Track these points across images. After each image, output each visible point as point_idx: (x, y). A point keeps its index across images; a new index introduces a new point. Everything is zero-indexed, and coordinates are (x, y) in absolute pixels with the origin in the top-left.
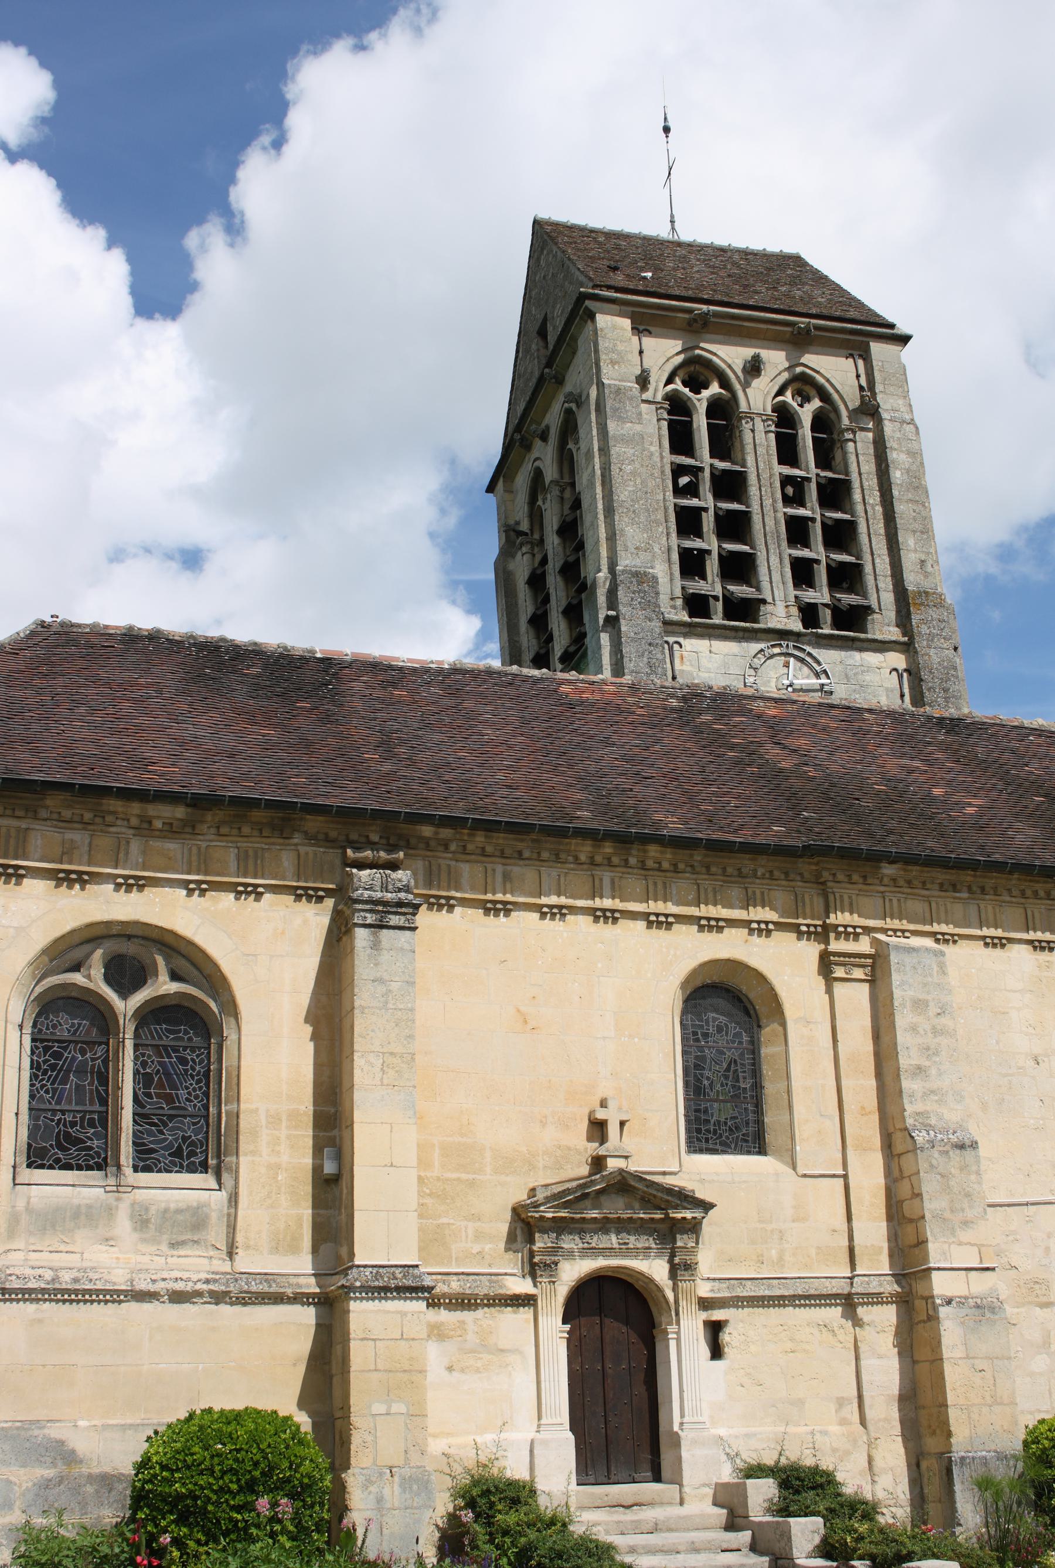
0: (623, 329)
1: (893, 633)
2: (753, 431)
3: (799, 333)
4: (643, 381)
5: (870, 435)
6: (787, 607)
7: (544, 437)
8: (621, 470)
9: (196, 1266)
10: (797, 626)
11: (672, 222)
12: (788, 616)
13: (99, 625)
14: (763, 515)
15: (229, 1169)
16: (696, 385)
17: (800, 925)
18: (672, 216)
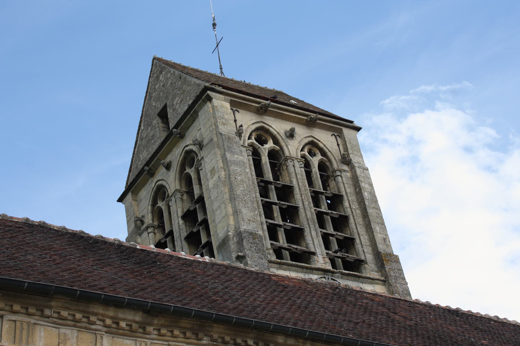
0: (226, 107)
1: (375, 275)
2: (294, 166)
3: (311, 120)
4: (239, 133)
5: (349, 174)
6: (323, 258)
7: (168, 167)
8: (236, 178)
10: (329, 267)
11: (221, 68)
12: (325, 263)
13: (7, 216)
14: (305, 209)
16: (262, 141)
18: (221, 66)
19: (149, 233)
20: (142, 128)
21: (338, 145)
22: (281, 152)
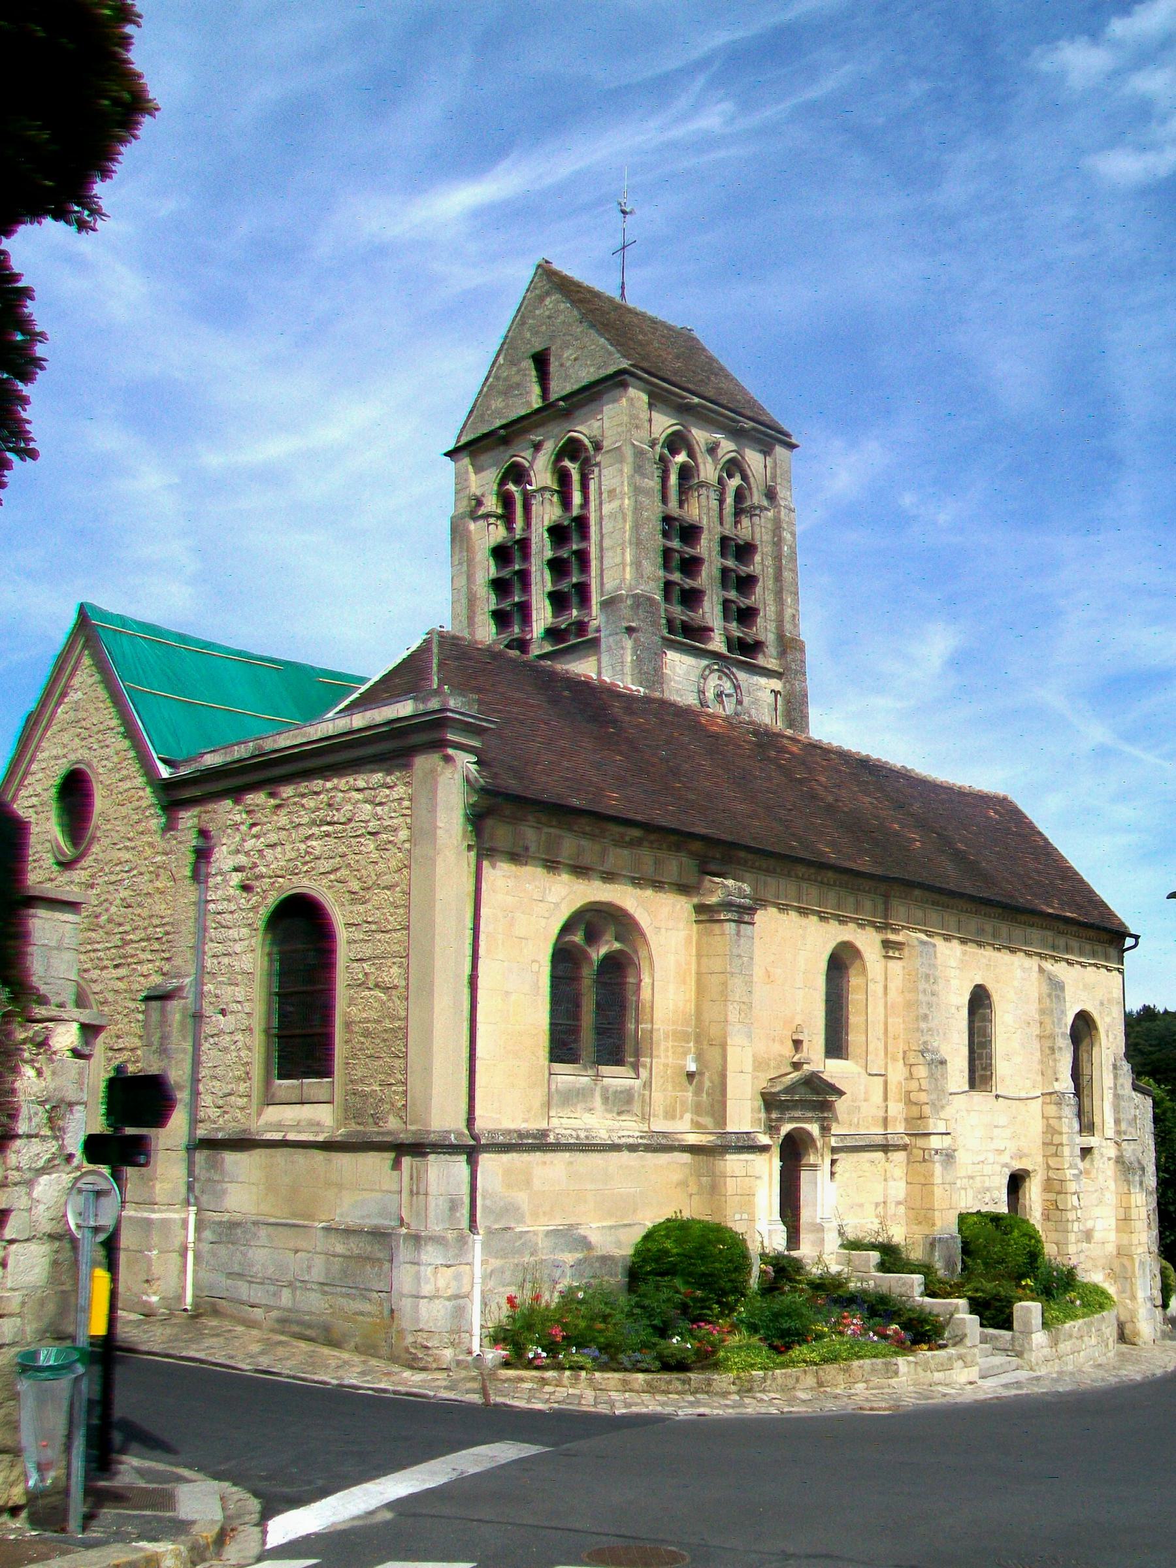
9: (629, 1128)
11: (623, 288)
15: (644, 1066)
16: (674, 452)
20: (501, 360)
22: (694, 470)
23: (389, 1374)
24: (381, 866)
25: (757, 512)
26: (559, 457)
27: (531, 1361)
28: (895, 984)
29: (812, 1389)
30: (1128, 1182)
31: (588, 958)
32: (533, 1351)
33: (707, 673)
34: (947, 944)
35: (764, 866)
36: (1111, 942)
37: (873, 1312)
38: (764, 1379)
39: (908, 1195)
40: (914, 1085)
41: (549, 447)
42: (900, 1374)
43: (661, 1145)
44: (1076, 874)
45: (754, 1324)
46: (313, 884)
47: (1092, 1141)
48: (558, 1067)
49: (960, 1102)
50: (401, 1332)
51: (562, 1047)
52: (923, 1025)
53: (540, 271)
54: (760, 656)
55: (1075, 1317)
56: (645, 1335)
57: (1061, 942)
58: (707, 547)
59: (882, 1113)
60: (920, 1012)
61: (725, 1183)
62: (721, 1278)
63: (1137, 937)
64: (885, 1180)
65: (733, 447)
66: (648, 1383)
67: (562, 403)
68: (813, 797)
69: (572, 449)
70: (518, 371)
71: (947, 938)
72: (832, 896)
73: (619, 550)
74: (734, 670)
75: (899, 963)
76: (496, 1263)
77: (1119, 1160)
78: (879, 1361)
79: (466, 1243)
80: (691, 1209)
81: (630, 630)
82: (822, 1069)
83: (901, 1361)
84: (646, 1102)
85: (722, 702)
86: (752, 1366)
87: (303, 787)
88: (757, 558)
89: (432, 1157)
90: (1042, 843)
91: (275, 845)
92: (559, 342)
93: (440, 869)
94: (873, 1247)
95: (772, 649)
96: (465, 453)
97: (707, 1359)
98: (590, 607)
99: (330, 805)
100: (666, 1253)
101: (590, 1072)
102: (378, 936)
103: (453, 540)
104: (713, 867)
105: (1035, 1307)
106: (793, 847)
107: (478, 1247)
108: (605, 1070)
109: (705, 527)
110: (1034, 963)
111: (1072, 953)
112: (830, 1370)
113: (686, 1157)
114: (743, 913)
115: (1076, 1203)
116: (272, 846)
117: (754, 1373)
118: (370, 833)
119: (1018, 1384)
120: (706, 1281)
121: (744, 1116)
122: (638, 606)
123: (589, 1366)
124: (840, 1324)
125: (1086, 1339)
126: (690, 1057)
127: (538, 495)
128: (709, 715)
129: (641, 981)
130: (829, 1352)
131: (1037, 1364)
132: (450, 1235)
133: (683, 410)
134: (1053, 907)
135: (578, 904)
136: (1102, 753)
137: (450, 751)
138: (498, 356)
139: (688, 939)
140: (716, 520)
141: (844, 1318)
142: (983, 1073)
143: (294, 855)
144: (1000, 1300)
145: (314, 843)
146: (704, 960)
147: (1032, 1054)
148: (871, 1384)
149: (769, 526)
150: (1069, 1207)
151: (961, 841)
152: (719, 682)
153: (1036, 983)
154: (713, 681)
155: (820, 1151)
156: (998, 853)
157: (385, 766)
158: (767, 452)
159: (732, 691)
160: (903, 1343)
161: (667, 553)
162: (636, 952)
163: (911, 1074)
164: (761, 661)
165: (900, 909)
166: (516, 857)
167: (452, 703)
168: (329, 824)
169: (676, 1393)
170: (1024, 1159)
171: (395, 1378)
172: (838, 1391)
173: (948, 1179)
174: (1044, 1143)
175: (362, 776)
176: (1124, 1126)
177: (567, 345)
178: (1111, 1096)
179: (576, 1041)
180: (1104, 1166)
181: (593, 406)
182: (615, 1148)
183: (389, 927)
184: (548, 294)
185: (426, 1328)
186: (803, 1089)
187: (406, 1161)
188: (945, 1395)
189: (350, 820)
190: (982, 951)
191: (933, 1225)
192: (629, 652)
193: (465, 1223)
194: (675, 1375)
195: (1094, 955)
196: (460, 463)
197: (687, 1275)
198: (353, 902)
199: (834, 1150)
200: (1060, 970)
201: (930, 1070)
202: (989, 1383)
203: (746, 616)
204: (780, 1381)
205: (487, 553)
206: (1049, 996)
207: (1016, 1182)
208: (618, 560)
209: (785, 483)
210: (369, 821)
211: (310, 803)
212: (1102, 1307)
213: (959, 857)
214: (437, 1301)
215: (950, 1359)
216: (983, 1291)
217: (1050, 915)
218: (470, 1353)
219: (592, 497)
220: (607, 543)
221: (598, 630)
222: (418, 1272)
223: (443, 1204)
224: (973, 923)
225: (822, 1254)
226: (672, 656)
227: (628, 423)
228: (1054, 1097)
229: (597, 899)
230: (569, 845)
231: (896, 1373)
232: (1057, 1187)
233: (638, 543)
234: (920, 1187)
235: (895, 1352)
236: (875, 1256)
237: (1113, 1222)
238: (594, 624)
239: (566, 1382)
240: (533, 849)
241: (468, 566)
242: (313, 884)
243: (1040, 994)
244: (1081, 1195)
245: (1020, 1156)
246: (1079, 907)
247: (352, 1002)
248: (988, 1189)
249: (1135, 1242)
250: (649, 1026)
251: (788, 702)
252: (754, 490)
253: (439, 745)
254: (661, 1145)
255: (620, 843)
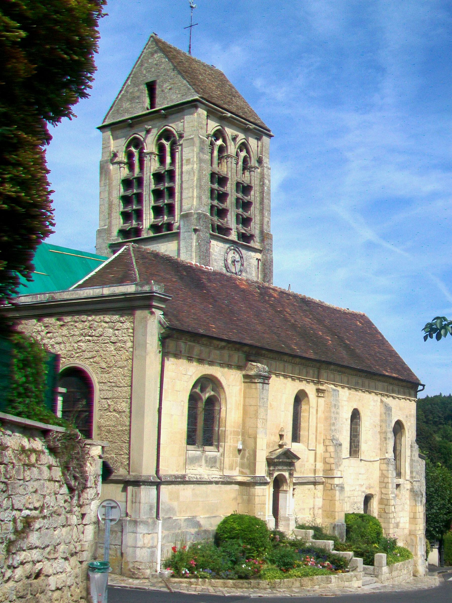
9: (215, 474)
11: (190, 48)
15: (222, 447)
16: (217, 139)
17: (314, 380)
18: (190, 45)
19: (120, 167)
21: (258, 146)
22: (225, 149)
23: (123, 580)
24: (118, 358)
25: (253, 170)
26: (160, 138)
27: (183, 575)
28: (321, 409)
29: (298, 587)
30: (415, 501)
31: (201, 398)
32: (184, 571)
33: (228, 250)
34: (343, 390)
35: (271, 357)
36: (412, 388)
37: (318, 557)
38: (280, 583)
39: (323, 505)
40: (328, 455)
41: (155, 133)
42: (332, 582)
43: (227, 482)
44: (396, 354)
45: (274, 560)
46: (81, 362)
47: (401, 481)
48: (190, 447)
49: (346, 462)
50: (127, 563)
51: (191, 440)
52: (333, 428)
53: (152, 39)
54: (252, 242)
55: (398, 561)
56: (230, 564)
57: (391, 387)
58: (230, 188)
59: (313, 467)
60: (331, 422)
61: (255, 499)
62: (257, 540)
63: (424, 386)
64: (314, 498)
65: (244, 137)
66: (234, 584)
67: (163, 111)
68: (286, 320)
69: (167, 135)
70: (138, 90)
71: (343, 387)
72: (297, 368)
73: (191, 190)
74: (240, 249)
75: (323, 399)
76: (166, 532)
77: (412, 490)
78: (324, 576)
79: (156, 524)
80: (241, 510)
81: (195, 230)
82: (290, 448)
83: (332, 576)
84: (222, 463)
85: (235, 265)
86: (275, 577)
87: (76, 318)
88: (252, 193)
89: (142, 487)
90: (381, 338)
91: (60, 343)
92: (161, 79)
93: (148, 361)
94: (311, 528)
95: (257, 238)
96: (109, 129)
97: (257, 575)
98: (174, 216)
99: (90, 328)
100: (234, 529)
101: (201, 449)
102: (116, 389)
103: (101, 173)
104: (252, 358)
105: (384, 555)
106: (282, 347)
107: (160, 525)
108: (207, 448)
109: (230, 178)
110: (378, 398)
111: (395, 393)
112: (306, 579)
113: (237, 487)
114: (265, 379)
115: (393, 510)
116: (60, 343)
117: (276, 580)
118: (111, 342)
119: (377, 588)
120: (251, 541)
121: (261, 470)
122: (200, 219)
123: (208, 577)
124: (305, 561)
125: (403, 570)
126: (240, 442)
127: (148, 156)
128: (239, 279)
129: (221, 408)
130: (304, 572)
131: (384, 580)
132: (150, 521)
133: (222, 119)
134: (387, 372)
135: (199, 375)
136: (370, 246)
137: (154, 310)
138: (127, 80)
139: (240, 390)
140: (235, 174)
141: (307, 558)
142: (355, 449)
143: (71, 348)
144: (368, 553)
145: (82, 344)
146: (247, 400)
147: (376, 440)
148: (321, 586)
149: (258, 176)
150: (391, 512)
151: (347, 339)
152: (233, 255)
153: (379, 407)
154: (231, 255)
155: (289, 484)
156: (363, 344)
157: (121, 313)
158: (259, 139)
159: (239, 259)
160: (332, 570)
161: (212, 191)
162: (220, 396)
163: (326, 450)
164: (252, 244)
165: (324, 373)
166: (177, 356)
167: (155, 288)
168: (90, 336)
169: (245, 588)
170: (371, 489)
171: (126, 582)
172: (309, 589)
173: (342, 498)
174: (380, 482)
175: (108, 316)
176: (414, 474)
177: (165, 81)
178: (409, 460)
179: (195, 435)
180: (405, 494)
181: (179, 115)
182: (210, 483)
183: (121, 385)
184: (156, 52)
185: (139, 560)
186: (282, 457)
187: (130, 488)
188: (351, 591)
189: (101, 335)
190: (357, 393)
191: (335, 518)
192: (194, 241)
193: (155, 516)
194: (244, 581)
195: (404, 394)
196: (105, 134)
197: (243, 538)
198: (102, 372)
199: (295, 484)
200: (389, 401)
201: (335, 448)
202: (366, 588)
203: (246, 222)
204: (286, 584)
205: (119, 182)
206: (385, 413)
207: (368, 499)
208: (190, 195)
209: (268, 156)
210: (111, 337)
211: (80, 325)
212: (408, 557)
213: (347, 347)
214: (144, 549)
215: (351, 577)
216: (360, 548)
217: (387, 376)
218: (156, 571)
219: (177, 161)
220: (184, 185)
221: (179, 228)
222: (136, 537)
223: (147, 508)
224: (354, 379)
225: (289, 531)
226: (213, 242)
227: (197, 126)
228: (385, 461)
229: (207, 373)
230: (197, 349)
231: (331, 582)
232: (385, 502)
233: (200, 187)
234: (329, 501)
235: (330, 573)
236: (311, 532)
237: (408, 519)
238: (176, 225)
239: (200, 583)
240: (183, 352)
241: (109, 187)
242: (81, 362)
243: (381, 413)
244: (396, 507)
245: (370, 487)
246: (398, 371)
247: (101, 417)
248: (356, 503)
249: (418, 528)
250: (224, 429)
251: (264, 265)
252: (252, 158)
253: (149, 307)
254: (227, 482)
255: (217, 348)
